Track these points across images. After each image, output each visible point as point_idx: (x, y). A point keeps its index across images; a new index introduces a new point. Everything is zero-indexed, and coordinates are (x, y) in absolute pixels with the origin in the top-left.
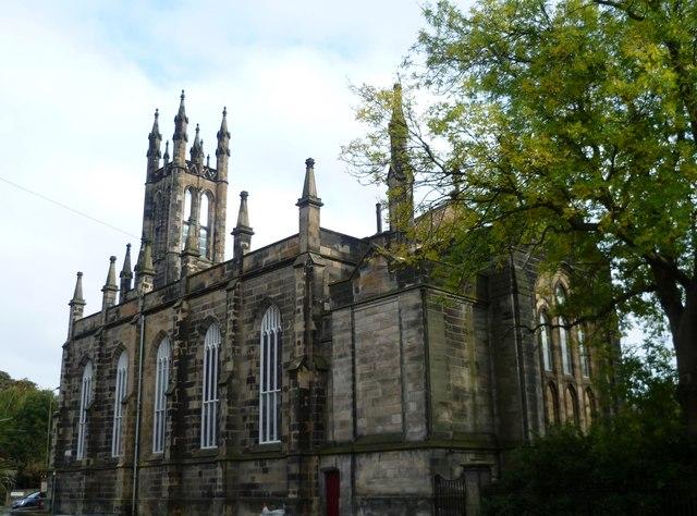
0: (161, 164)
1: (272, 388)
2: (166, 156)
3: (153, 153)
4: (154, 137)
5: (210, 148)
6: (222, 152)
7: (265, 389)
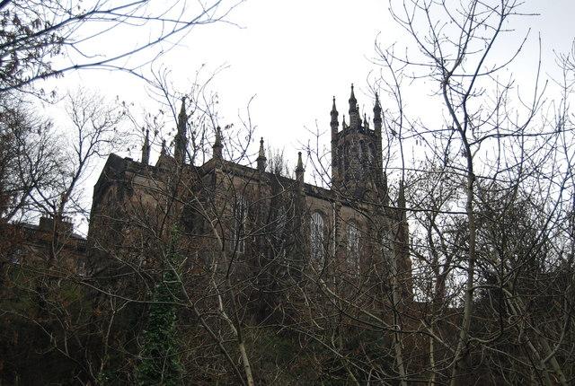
0: (340, 128)
2: (344, 123)
3: (334, 123)
4: (334, 113)
5: (371, 115)
6: (378, 120)
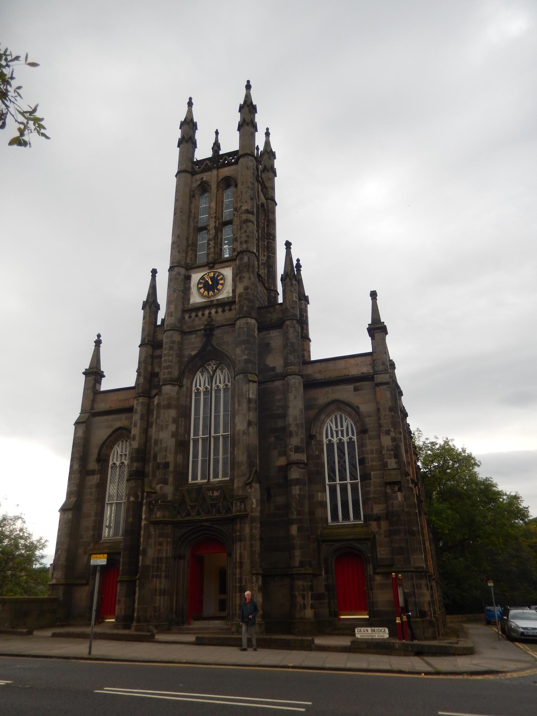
1: (343, 478)
7: (332, 478)
